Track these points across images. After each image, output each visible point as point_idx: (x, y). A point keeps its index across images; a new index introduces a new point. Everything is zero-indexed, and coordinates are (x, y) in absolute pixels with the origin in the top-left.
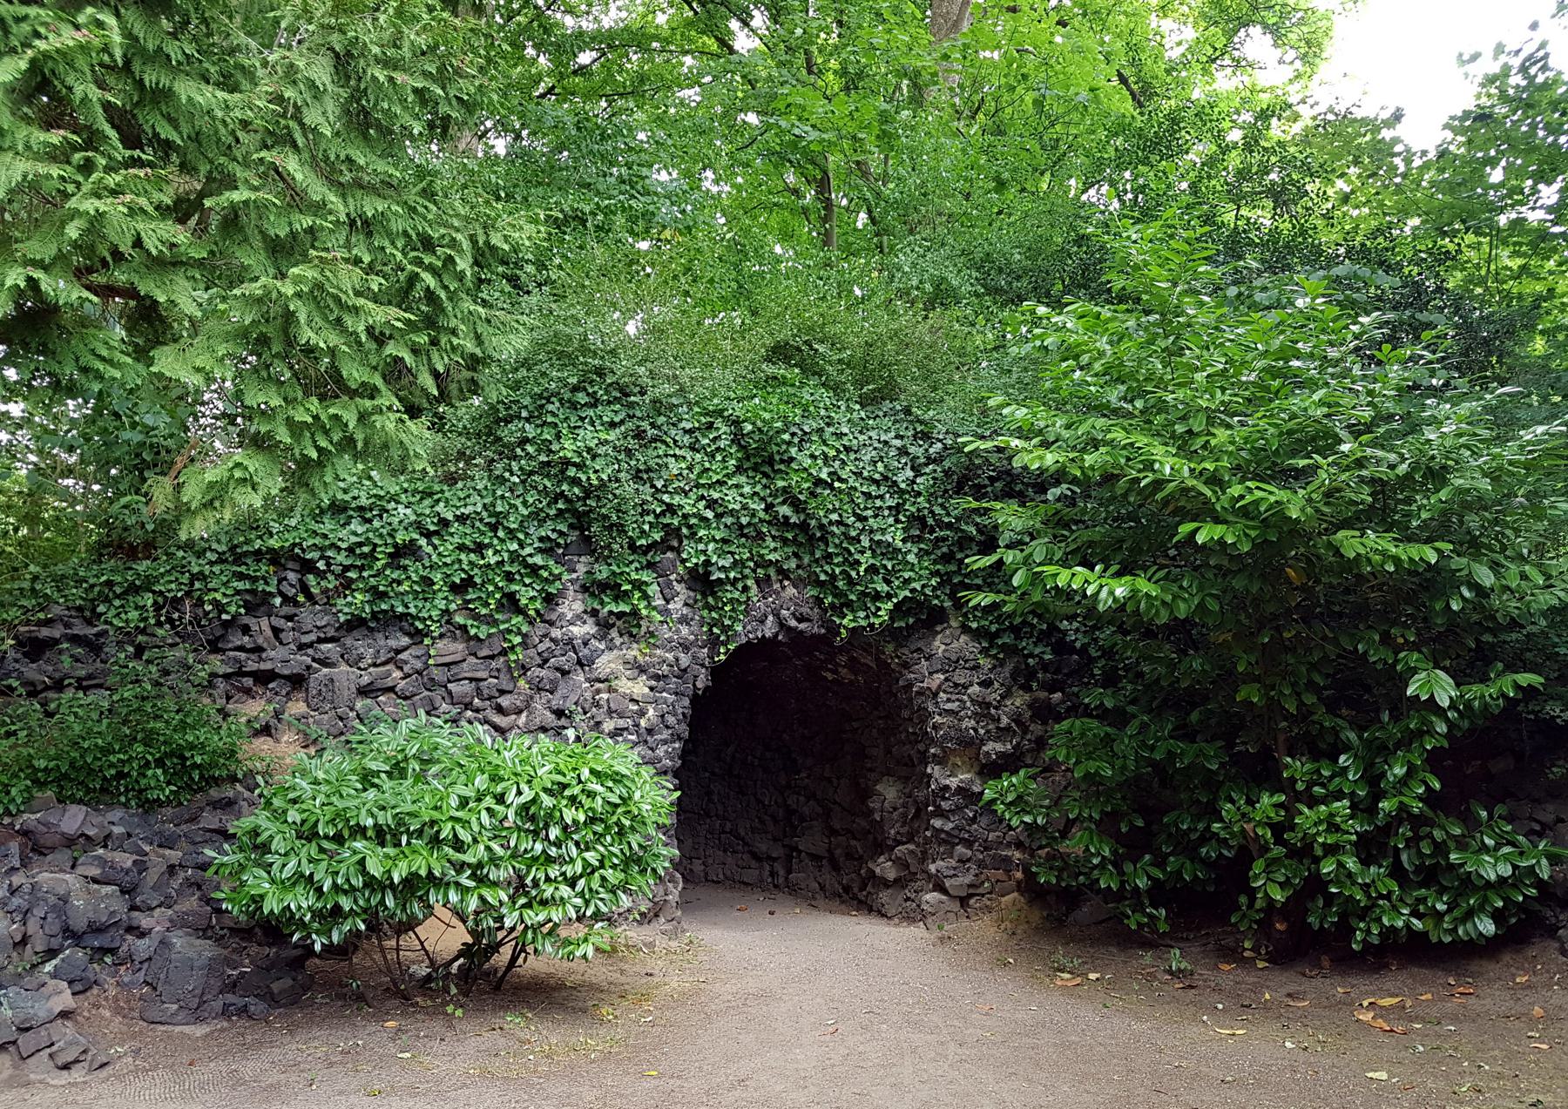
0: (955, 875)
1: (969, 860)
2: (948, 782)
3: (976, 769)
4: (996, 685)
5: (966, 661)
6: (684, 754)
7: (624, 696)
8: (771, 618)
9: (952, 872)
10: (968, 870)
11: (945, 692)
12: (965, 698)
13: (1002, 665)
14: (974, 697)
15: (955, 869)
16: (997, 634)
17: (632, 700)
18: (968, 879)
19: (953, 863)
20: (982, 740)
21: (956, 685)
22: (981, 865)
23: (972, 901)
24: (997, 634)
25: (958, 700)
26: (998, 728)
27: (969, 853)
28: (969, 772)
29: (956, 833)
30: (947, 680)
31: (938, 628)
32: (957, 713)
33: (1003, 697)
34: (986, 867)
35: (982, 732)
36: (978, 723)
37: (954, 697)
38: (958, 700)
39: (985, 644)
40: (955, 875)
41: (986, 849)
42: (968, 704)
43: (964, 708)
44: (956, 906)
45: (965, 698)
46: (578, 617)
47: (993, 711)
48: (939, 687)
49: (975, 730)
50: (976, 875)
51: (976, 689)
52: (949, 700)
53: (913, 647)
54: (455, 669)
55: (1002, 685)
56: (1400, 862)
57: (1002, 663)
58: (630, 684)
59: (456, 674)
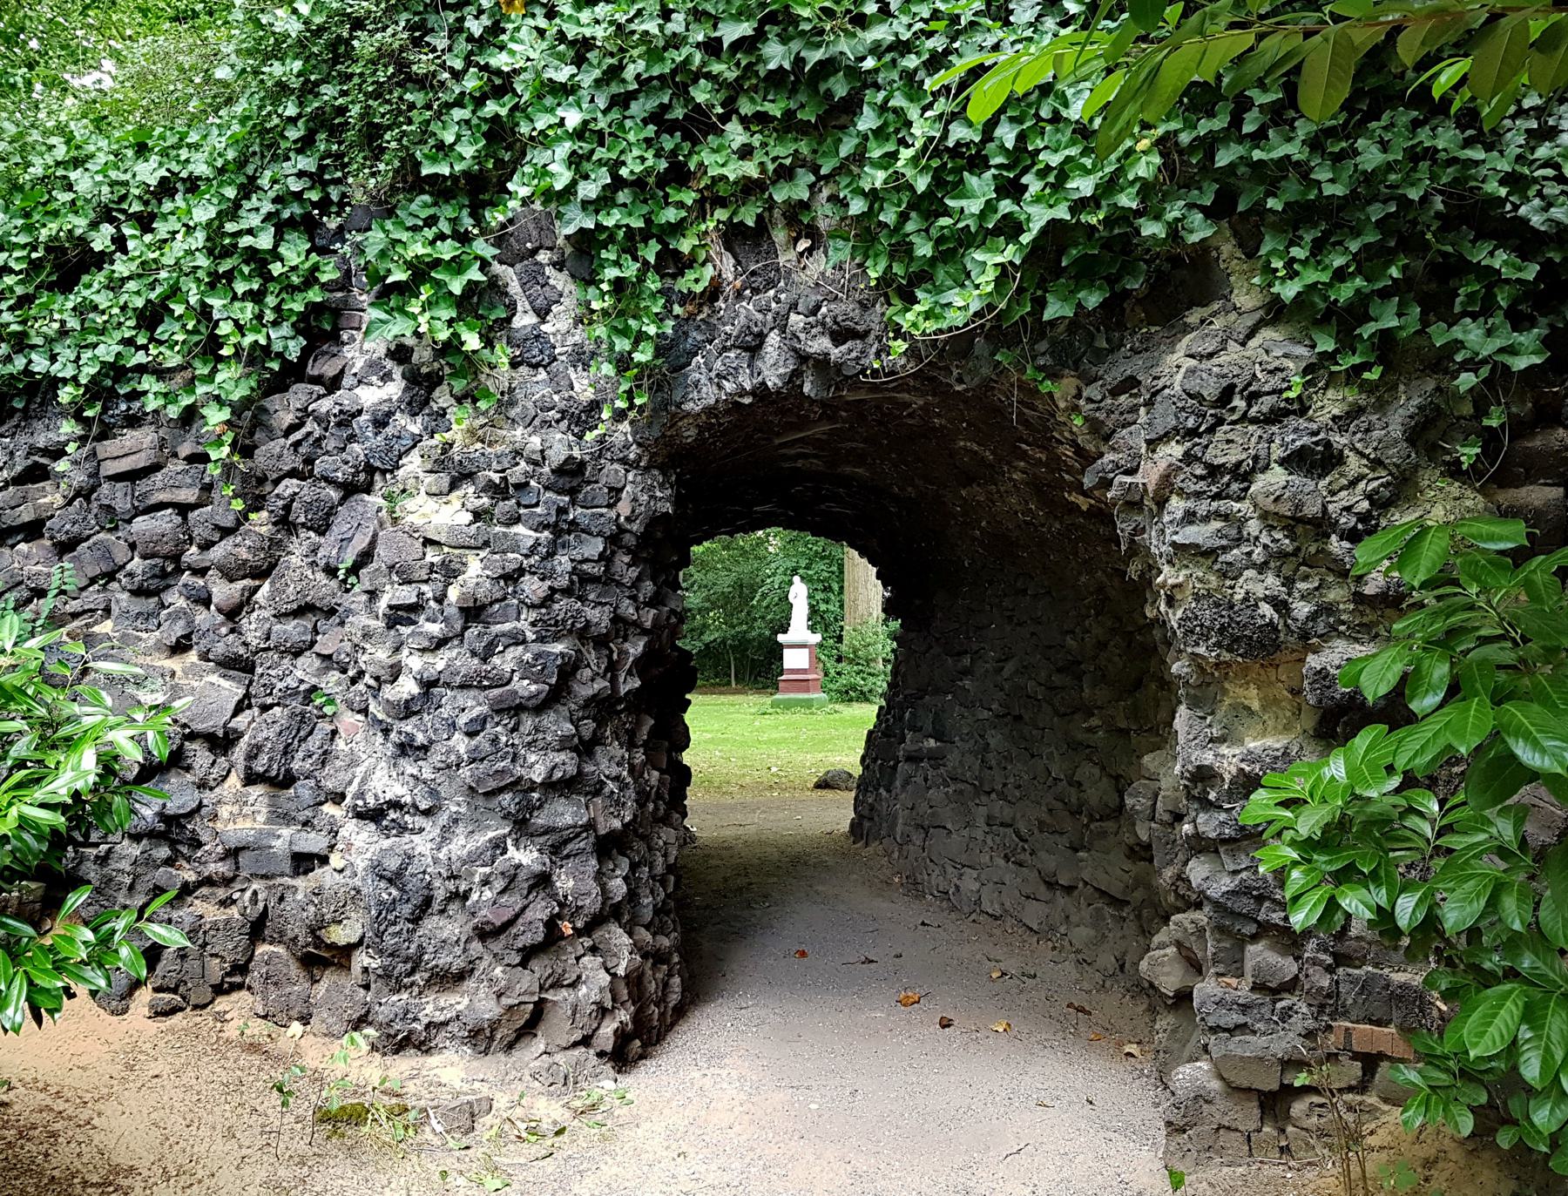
0: (1241, 1028)
1: (1291, 986)
2: (1208, 758)
3: (1308, 721)
4: (1354, 465)
5: (1252, 398)
6: (895, 673)
7: (412, 531)
8: (773, 339)
9: (1236, 1018)
10: (1286, 1014)
11: (1181, 493)
12: (1244, 507)
13: (1381, 406)
14: (1268, 503)
15: (1245, 1008)
16: (1358, 311)
17: (428, 542)
18: (1285, 1042)
19: (1243, 990)
20: (1304, 636)
21: (1214, 471)
22: (1328, 1005)
23: (1298, 1108)
24: (1358, 311)
25: (1217, 515)
26: (1358, 598)
27: (1289, 967)
28: (1287, 728)
29: (1244, 905)
30: (1188, 458)
31: (1193, 317)
32: (1211, 553)
33: (1381, 503)
34: (1340, 1012)
35: (1302, 609)
36: (1289, 583)
37: (1203, 507)
38: (1217, 515)
39: (1326, 344)
40: (1241, 1028)
41: (1341, 959)
42: (1253, 527)
43: (1239, 541)
44: (1247, 1116)
45: (1244, 507)
46: (373, 366)
47: (1336, 545)
48: (1166, 480)
49: (1281, 606)
50: (1309, 1035)
51: (1276, 477)
52: (1190, 517)
53: (1114, 376)
54: (143, 486)
55: (1376, 463)
56: (1529, 479)
57: (1382, 397)
58: (431, 504)
59: (145, 495)
